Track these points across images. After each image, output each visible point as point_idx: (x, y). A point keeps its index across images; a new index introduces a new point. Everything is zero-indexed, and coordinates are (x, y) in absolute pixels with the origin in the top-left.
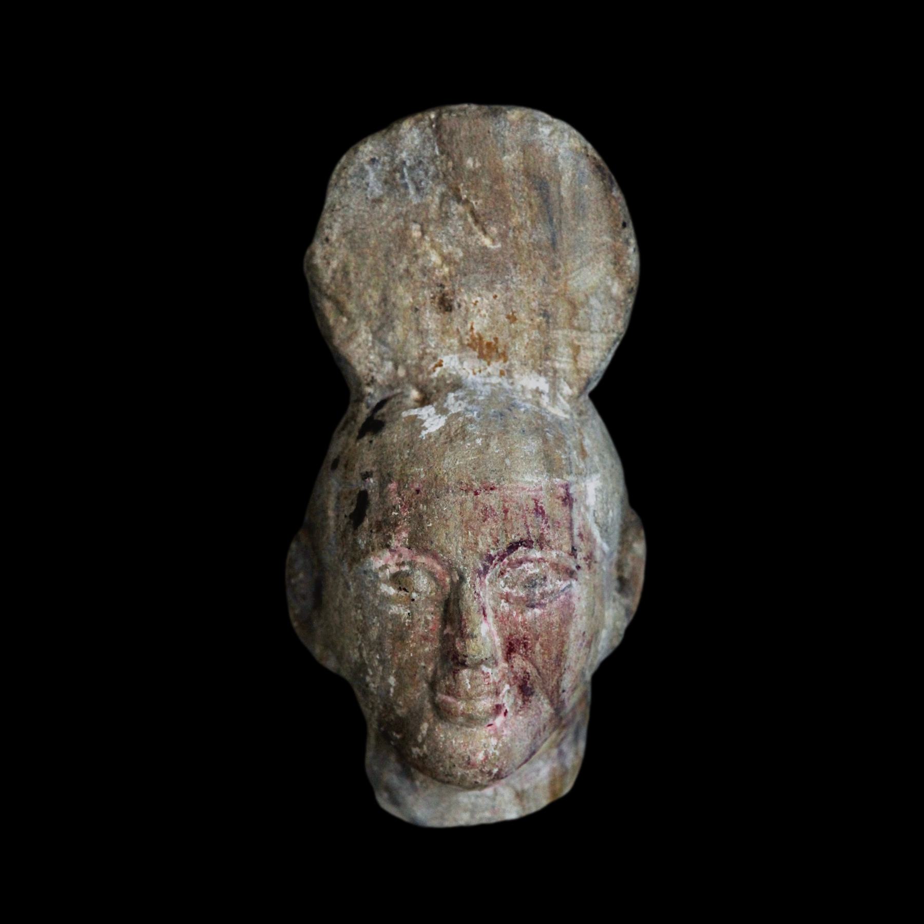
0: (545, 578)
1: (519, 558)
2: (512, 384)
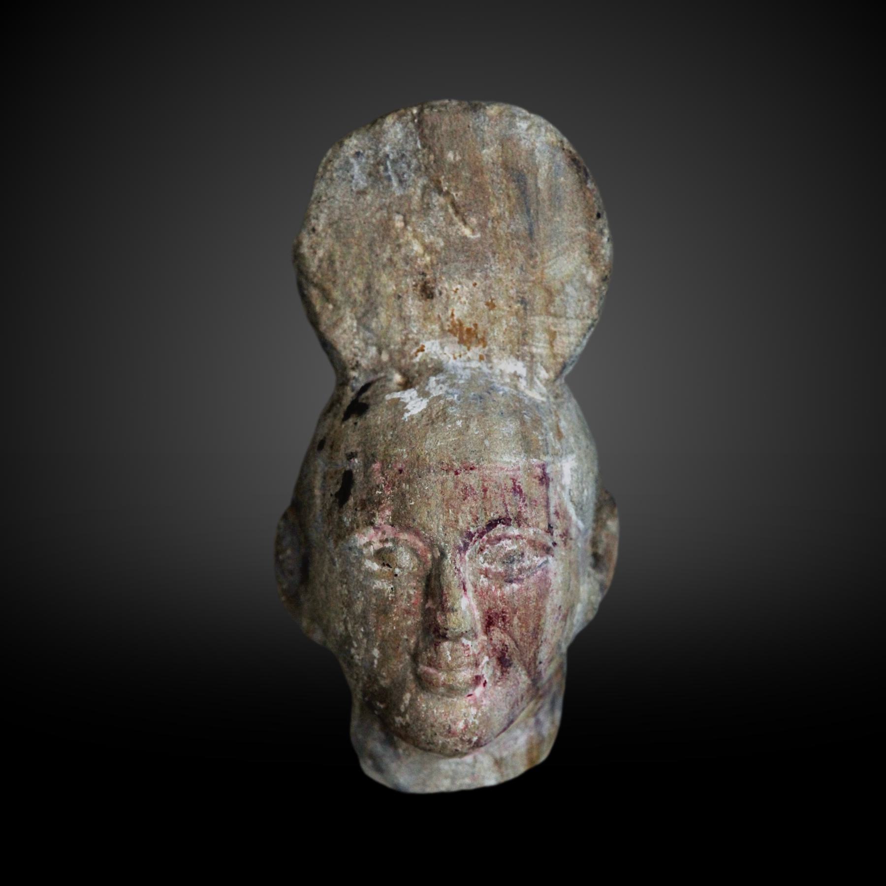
0: (522, 554)
1: (498, 535)
2: (491, 368)
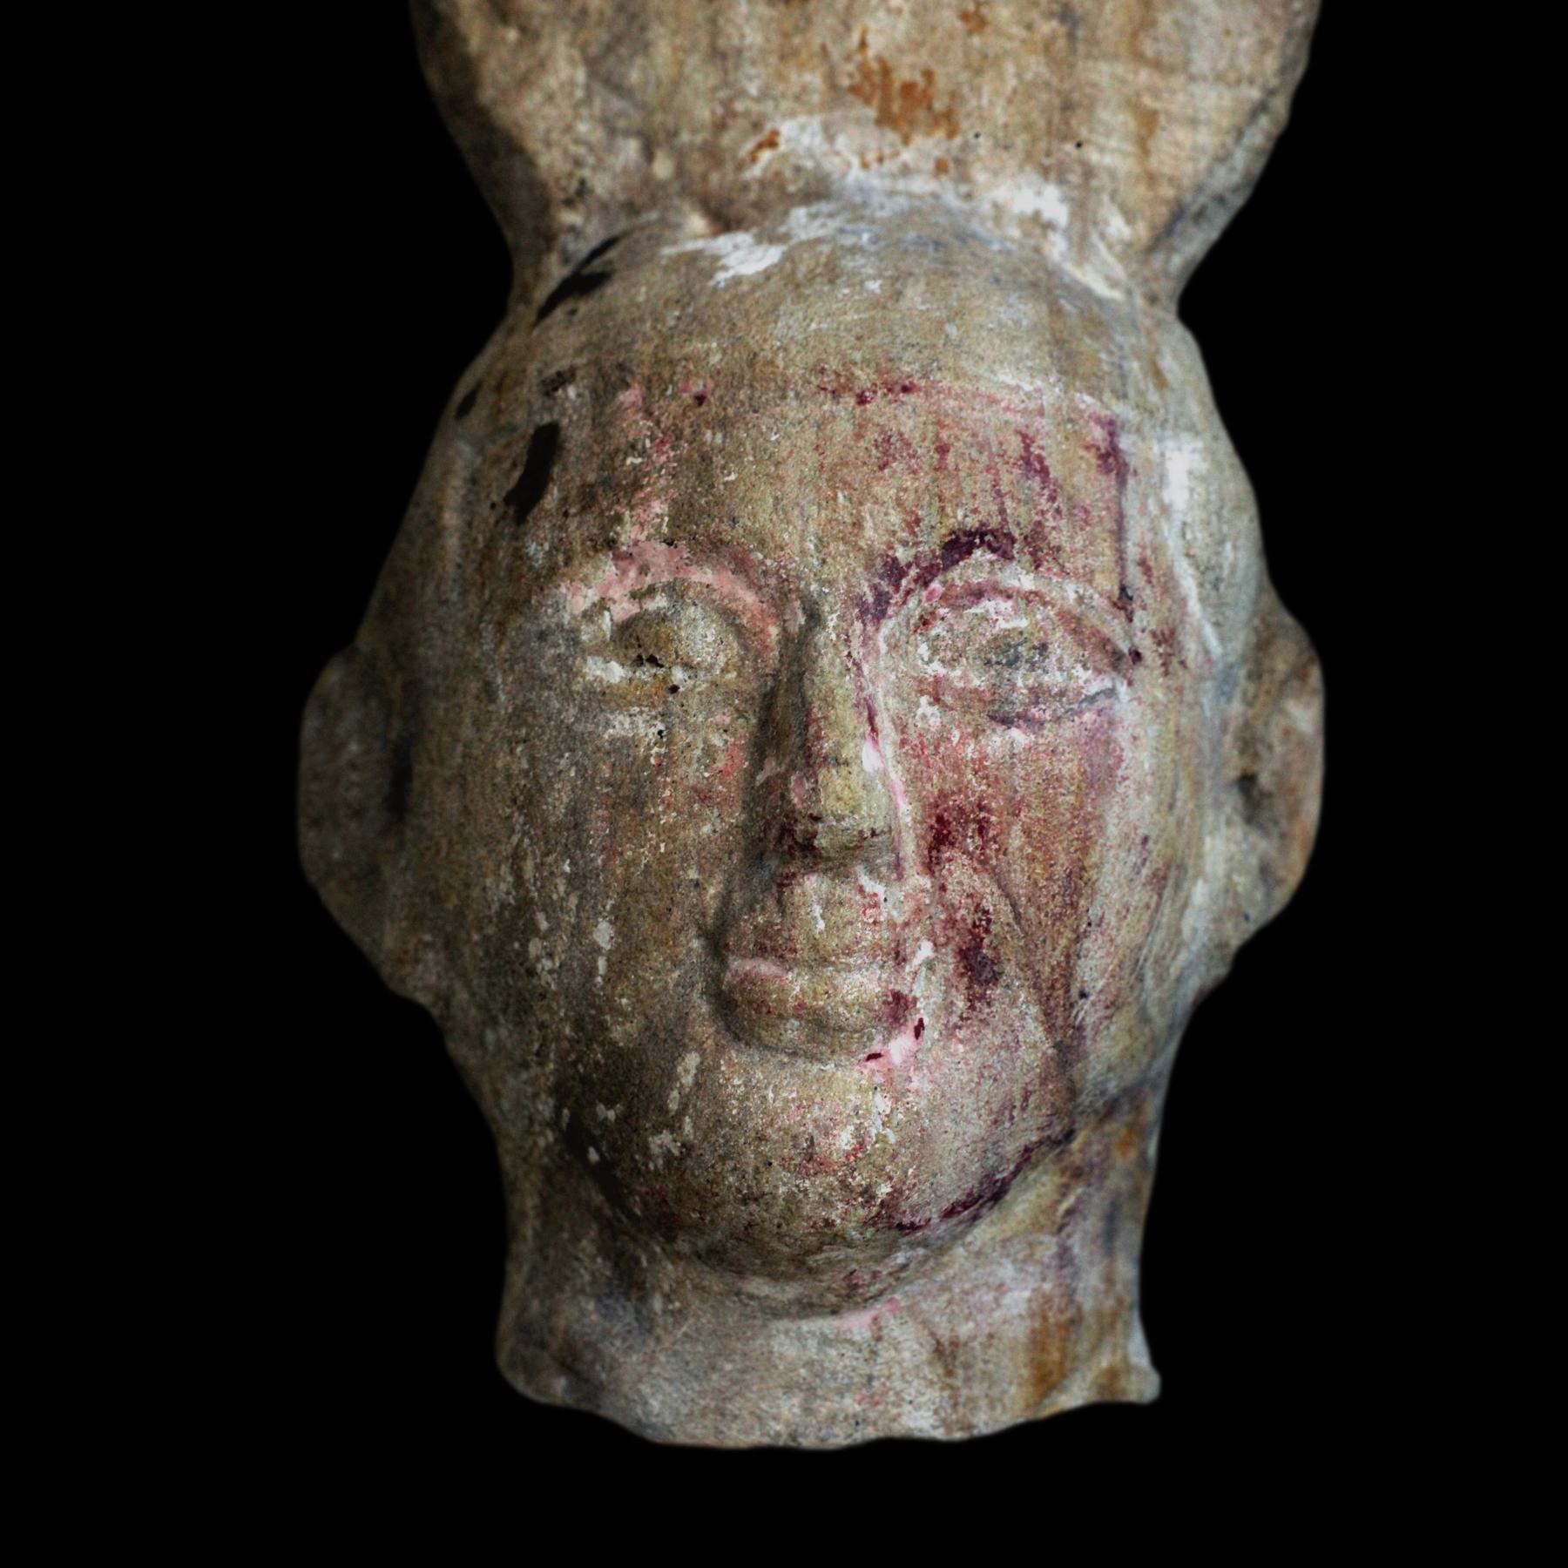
0: (1043, 648)
1: (975, 581)
2: (969, 196)
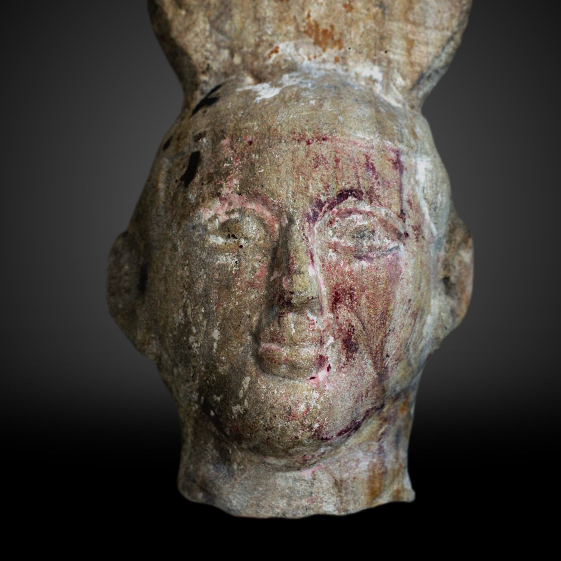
0: (373, 232)
1: (349, 208)
2: (347, 70)
